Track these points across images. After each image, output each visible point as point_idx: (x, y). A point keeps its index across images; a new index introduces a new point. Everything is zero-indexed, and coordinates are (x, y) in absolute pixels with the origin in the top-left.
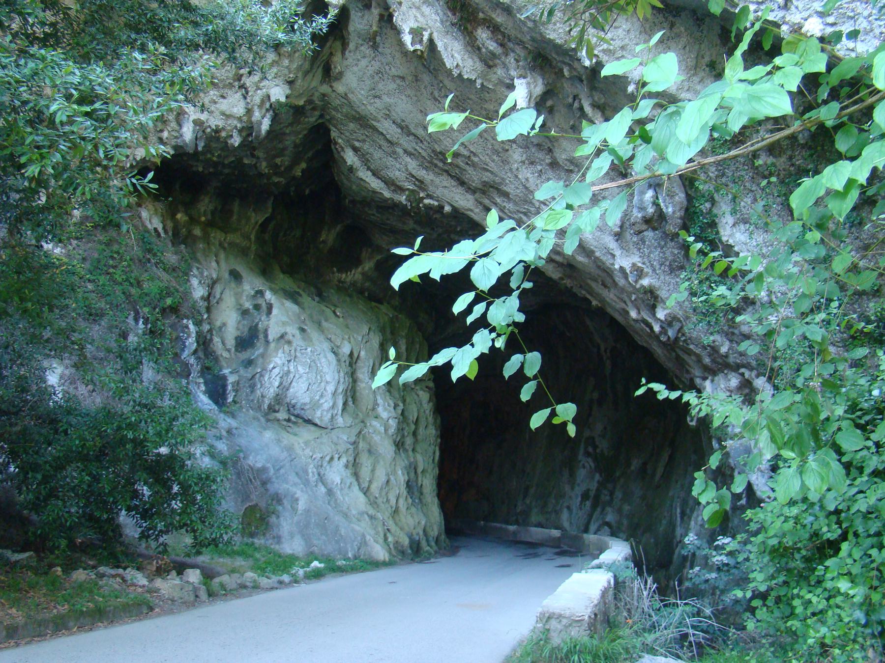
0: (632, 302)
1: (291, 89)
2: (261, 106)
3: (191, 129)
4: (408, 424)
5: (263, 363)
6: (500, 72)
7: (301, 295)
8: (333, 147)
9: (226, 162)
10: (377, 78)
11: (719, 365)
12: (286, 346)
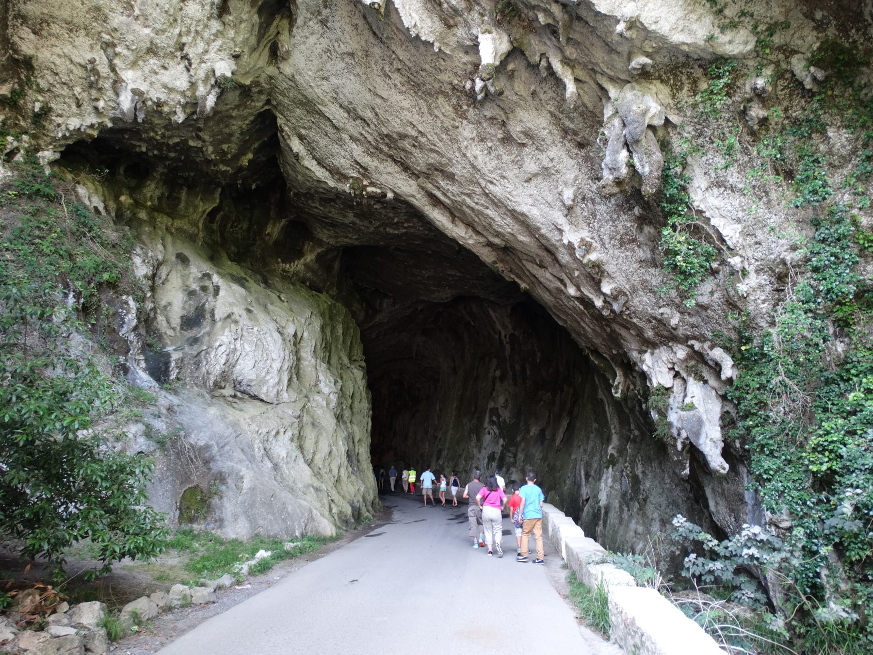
1: (236, 64)
2: (206, 80)
3: (129, 98)
4: (346, 399)
5: (209, 341)
6: (460, 32)
8: (279, 134)
9: (171, 142)
11: (667, 337)
12: (232, 325)
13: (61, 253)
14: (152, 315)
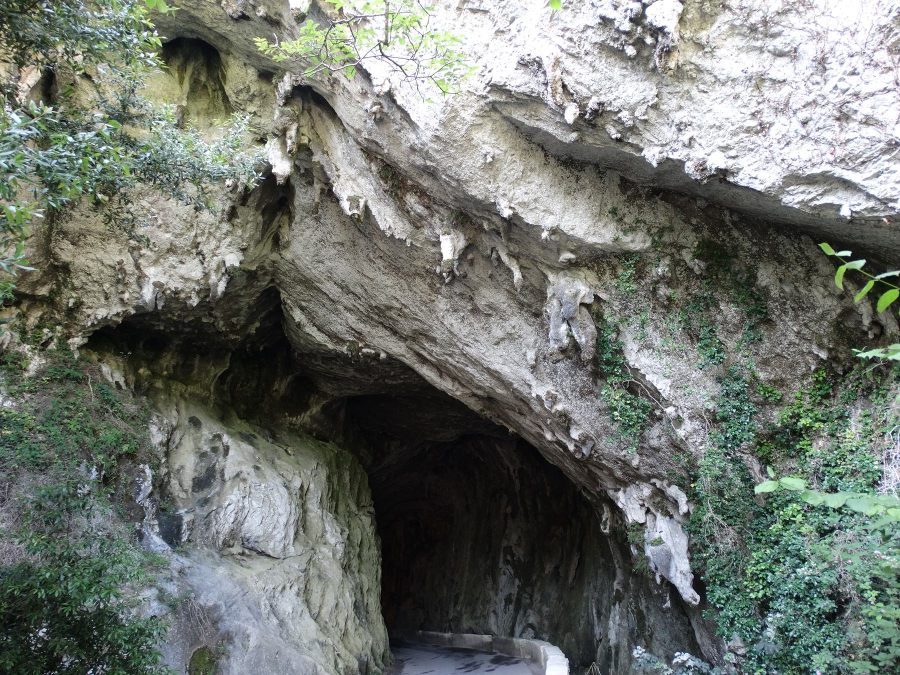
0: (547, 425)
2: (217, 270)
3: (151, 290)
6: (427, 231)
7: (256, 438)
9: (186, 321)
10: (319, 245)
11: (632, 477)
12: (241, 484)
13: (87, 430)
14: (166, 480)
